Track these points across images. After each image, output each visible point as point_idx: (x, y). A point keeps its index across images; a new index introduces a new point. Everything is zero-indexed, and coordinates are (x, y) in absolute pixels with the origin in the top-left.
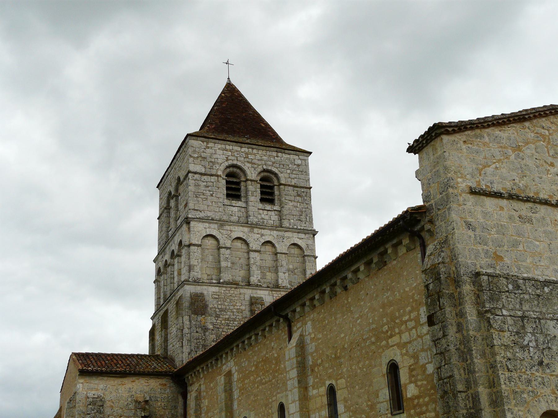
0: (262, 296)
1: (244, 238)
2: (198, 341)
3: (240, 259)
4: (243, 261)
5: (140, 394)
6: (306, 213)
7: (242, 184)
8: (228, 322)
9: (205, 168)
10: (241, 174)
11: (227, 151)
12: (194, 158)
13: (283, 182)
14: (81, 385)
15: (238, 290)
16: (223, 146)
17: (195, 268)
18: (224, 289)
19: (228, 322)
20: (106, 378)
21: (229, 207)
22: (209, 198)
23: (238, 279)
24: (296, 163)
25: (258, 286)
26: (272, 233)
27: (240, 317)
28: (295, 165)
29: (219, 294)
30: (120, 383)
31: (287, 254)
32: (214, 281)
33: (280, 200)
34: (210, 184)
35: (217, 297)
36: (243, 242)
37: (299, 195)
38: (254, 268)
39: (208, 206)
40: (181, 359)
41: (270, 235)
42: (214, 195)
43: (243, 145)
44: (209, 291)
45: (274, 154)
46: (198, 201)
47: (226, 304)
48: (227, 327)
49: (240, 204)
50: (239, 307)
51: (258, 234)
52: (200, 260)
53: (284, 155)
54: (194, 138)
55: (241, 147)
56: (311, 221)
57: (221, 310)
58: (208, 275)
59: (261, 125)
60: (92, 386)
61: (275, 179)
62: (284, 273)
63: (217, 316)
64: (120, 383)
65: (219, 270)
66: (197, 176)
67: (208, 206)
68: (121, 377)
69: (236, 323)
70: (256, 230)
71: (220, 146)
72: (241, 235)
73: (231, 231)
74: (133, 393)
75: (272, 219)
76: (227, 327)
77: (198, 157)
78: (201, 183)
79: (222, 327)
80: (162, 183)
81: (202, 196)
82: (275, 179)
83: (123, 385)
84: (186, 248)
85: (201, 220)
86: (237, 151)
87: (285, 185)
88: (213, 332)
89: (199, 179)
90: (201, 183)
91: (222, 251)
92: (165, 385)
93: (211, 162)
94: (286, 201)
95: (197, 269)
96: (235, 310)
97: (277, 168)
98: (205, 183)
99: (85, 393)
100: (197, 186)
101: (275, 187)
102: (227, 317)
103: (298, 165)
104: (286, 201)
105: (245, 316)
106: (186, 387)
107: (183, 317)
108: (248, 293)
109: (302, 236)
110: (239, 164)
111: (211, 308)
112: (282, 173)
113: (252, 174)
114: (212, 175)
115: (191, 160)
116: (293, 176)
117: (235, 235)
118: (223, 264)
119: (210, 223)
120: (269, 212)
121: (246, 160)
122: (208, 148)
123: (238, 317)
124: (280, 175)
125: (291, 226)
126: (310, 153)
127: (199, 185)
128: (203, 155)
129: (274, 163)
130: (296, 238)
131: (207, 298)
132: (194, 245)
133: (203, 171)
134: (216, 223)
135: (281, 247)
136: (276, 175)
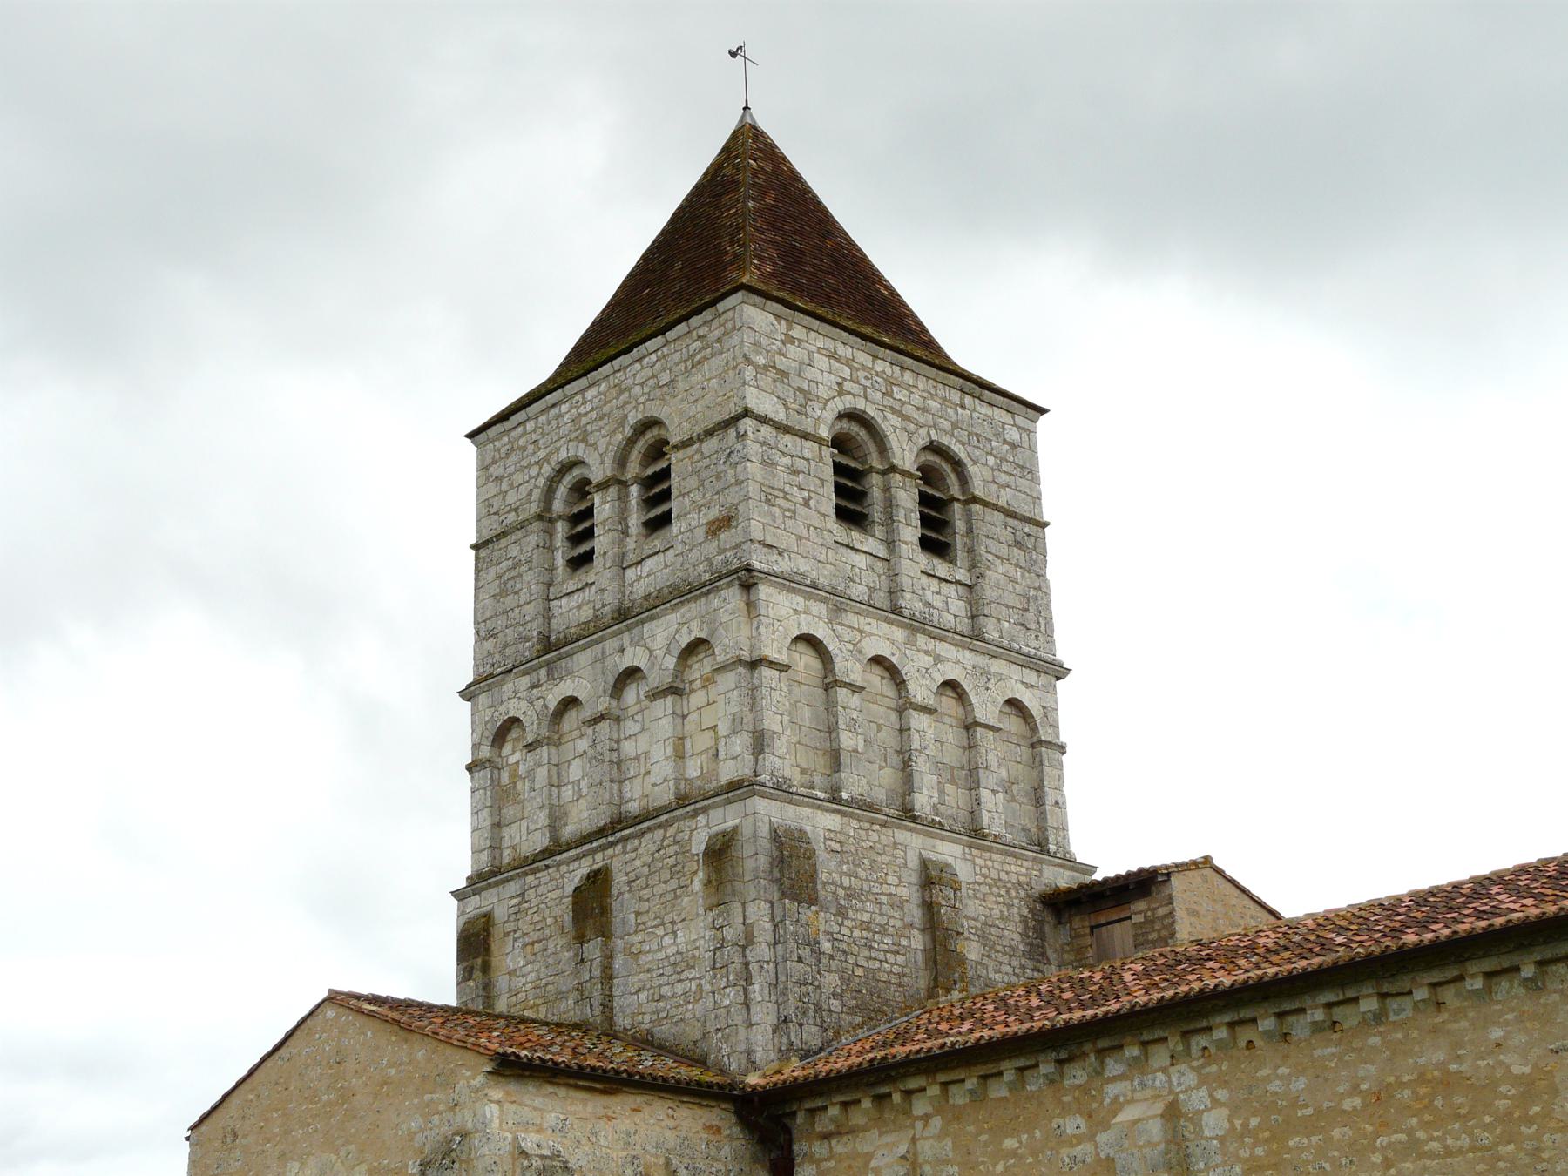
0: (950, 860)
1: (894, 660)
2: (804, 989)
3: (879, 729)
4: (888, 738)
5: (656, 1156)
6: (1034, 606)
7: (875, 480)
8: (870, 935)
9: (787, 408)
10: (871, 447)
11: (838, 361)
12: (757, 367)
13: (979, 492)
14: (495, 1107)
15: (890, 832)
16: (829, 344)
17: (777, 743)
18: (854, 823)
19: (870, 935)
20: (562, 1092)
21: (844, 550)
22: (801, 510)
23: (879, 795)
24: (1007, 437)
25: (934, 826)
26: (960, 657)
27: (898, 924)
28: (1005, 442)
29: (840, 837)
30: (601, 1112)
31: (997, 730)
32: (822, 795)
33: (971, 551)
34: (801, 464)
35: (837, 847)
36: (887, 675)
37: (1018, 544)
38: (921, 765)
39: (799, 538)
40: (742, 1047)
41: (957, 662)
42: (812, 503)
43: (881, 351)
44: (820, 824)
45: (955, 396)
46: (773, 516)
47: (863, 874)
48: (866, 953)
49: (871, 544)
50: (892, 890)
51: (927, 652)
52: (786, 718)
53: (985, 410)
54: (757, 299)
55: (875, 357)
56: (1045, 630)
57: (852, 894)
58: (803, 772)
59: (878, 291)
60: (527, 1114)
61: (952, 480)
62: (994, 792)
63: (842, 913)
64: (601, 1112)
65: (835, 759)
66: (766, 431)
67: (799, 538)
68: (604, 1092)
69: (888, 940)
70: (922, 640)
71: (821, 342)
72: (884, 650)
73: (861, 632)
74: (638, 1151)
75: (953, 609)
76: (866, 953)
77: (766, 367)
78: (777, 457)
79: (855, 949)
80: (507, 425)
81: (780, 502)
82: (952, 480)
83: (610, 1118)
84: (741, 670)
85: (789, 582)
86: (864, 368)
87: (985, 504)
88: (834, 965)
89: (771, 442)
90: (777, 457)
91: (842, 694)
92: (719, 1130)
93: (801, 390)
94: (991, 557)
95: (780, 745)
96: (884, 899)
97: (963, 444)
98: (787, 460)
99: (509, 1136)
100: (768, 464)
101: (956, 505)
102: (866, 917)
103: (1014, 446)
104: (991, 557)
105: (908, 920)
106: (790, 1142)
107: (744, 904)
108: (913, 844)
109: (1031, 677)
110: (871, 411)
111: (824, 884)
112: (975, 463)
113: (906, 455)
114: (805, 436)
115: (749, 372)
116: (1003, 479)
117: (874, 647)
118: (847, 740)
119: (808, 597)
120: (943, 585)
121: (888, 401)
122: (792, 340)
123: (892, 922)
124: (972, 469)
125: (1005, 643)
126: (1042, 411)
127: (773, 464)
128: (781, 363)
129: (955, 425)
130: (1018, 684)
131: (810, 855)
132: (772, 664)
133: (780, 415)
134: (824, 600)
135: (986, 707)
136: (957, 465)
